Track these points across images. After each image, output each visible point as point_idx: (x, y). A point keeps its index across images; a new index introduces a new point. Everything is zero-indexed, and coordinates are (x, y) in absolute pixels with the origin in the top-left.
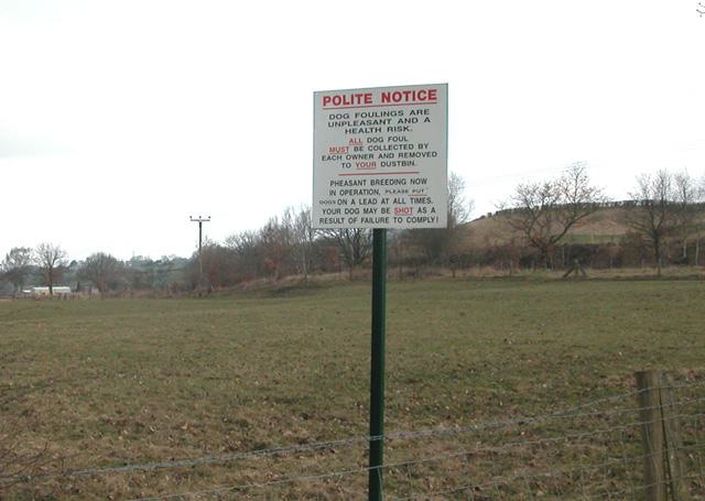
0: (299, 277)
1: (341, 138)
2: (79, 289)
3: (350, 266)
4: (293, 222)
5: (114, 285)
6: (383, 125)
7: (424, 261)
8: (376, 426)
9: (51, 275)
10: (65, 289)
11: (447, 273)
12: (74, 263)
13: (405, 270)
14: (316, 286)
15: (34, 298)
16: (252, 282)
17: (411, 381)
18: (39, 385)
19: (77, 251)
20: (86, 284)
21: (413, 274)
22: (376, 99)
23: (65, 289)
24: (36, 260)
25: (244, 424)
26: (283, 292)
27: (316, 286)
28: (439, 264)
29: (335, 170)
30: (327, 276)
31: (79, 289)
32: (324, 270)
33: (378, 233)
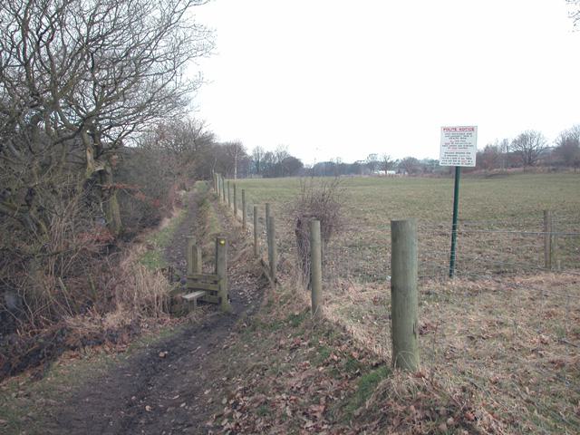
0: (499, 170)
1: (448, 140)
2: (399, 172)
3: (525, 164)
4: (499, 144)
5: (415, 171)
6: (460, 135)
7: (561, 164)
8: (454, 222)
9: (387, 166)
10: (393, 172)
11: (572, 170)
12: (397, 160)
13: (551, 167)
14: (508, 174)
15: (379, 176)
16: (478, 171)
17: (513, 215)
18: (372, 211)
19: (397, 155)
20: (402, 170)
21: (554, 170)
22: (458, 129)
23: (393, 172)
24: (380, 159)
25: (441, 227)
26: (491, 176)
27: (508, 174)
28: (568, 166)
29: (446, 149)
30: (513, 170)
31: (399, 172)
32: (512, 167)
33: (457, 167)
